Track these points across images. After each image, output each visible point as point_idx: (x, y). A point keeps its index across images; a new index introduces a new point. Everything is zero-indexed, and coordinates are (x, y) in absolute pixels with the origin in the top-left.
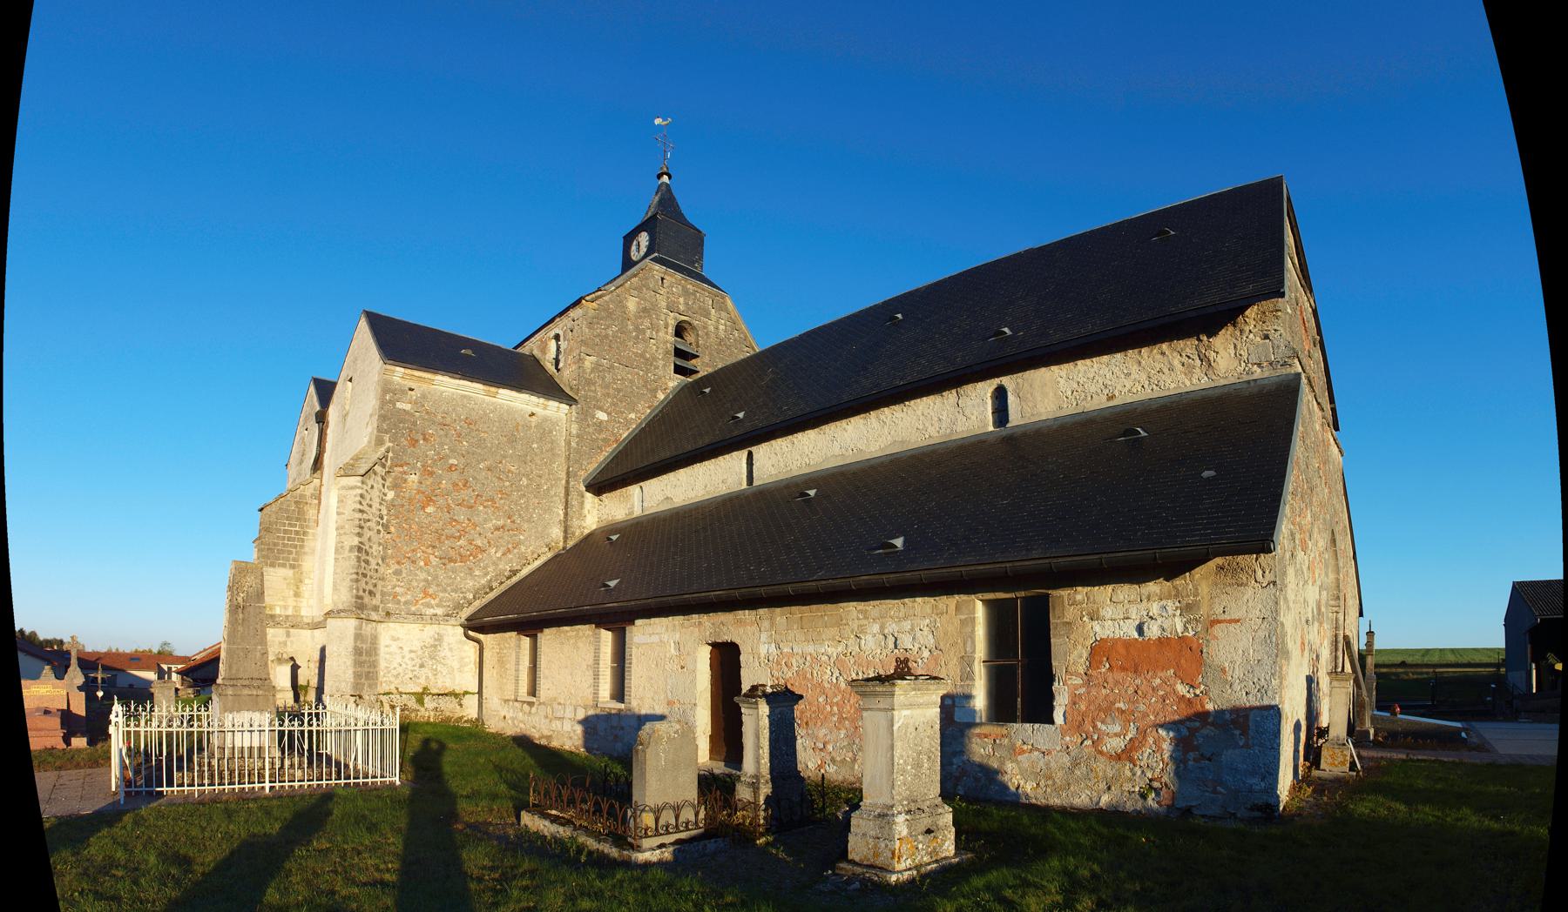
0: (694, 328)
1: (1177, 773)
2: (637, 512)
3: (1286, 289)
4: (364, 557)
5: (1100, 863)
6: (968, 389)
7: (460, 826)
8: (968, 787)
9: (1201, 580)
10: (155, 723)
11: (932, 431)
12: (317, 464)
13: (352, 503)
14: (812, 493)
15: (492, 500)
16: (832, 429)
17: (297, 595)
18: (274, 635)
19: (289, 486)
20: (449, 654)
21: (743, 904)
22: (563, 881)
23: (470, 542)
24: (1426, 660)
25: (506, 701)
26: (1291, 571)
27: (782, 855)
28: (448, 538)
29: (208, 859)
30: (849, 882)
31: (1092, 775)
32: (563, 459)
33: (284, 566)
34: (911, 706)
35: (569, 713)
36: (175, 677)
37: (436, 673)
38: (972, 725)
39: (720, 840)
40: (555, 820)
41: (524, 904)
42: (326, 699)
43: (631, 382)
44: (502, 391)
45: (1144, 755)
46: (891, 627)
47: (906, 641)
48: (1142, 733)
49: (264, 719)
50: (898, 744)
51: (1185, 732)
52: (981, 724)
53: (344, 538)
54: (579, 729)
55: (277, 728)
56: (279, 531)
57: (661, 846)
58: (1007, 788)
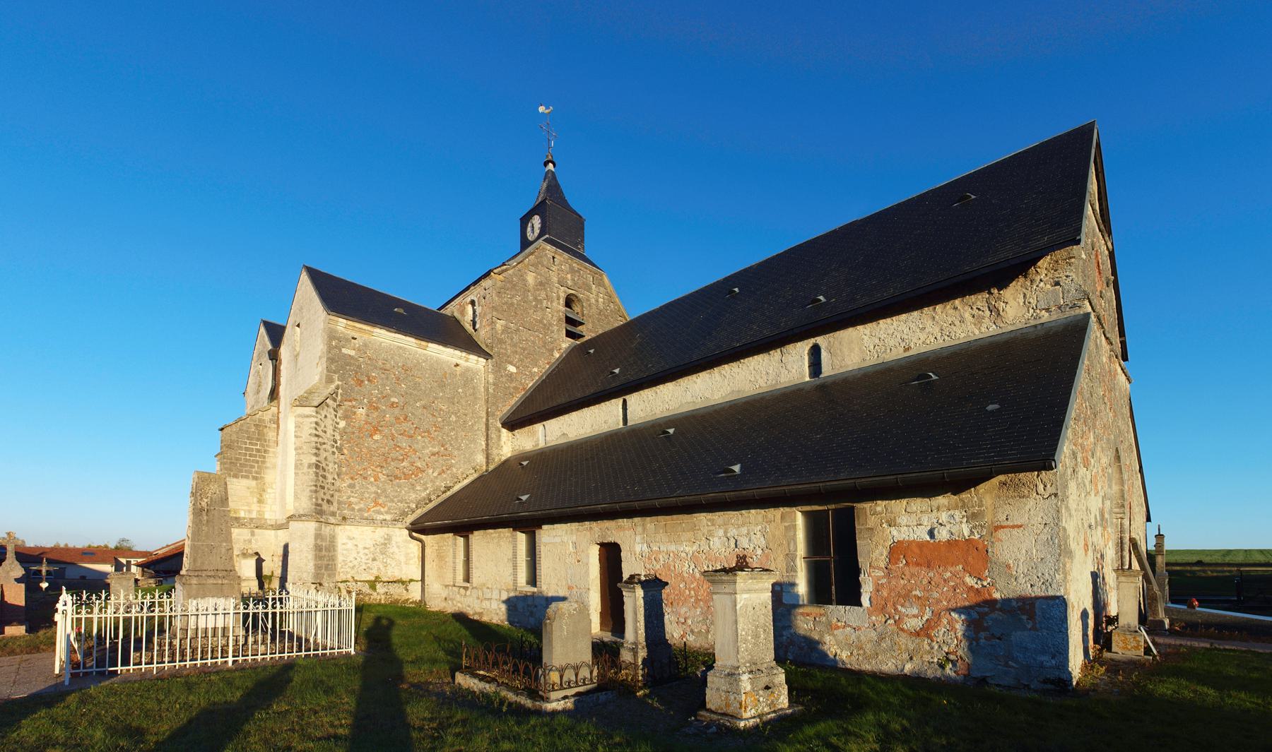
0: (579, 300)
1: (970, 648)
2: (542, 445)
3: (1083, 237)
4: (321, 473)
5: (909, 720)
6: (790, 348)
7: (405, 686)
8: (795, 653)
9: (986, 494)
10: (111, 610)
11: (762, 382)
12: (274, 394)
13: (308, 428)
15: (428, 432)
17: (260, 501)
19: (248, 411)
20: (396, 550)
21: (628, 744)
22: (489, 728)
23: (412, 464)
24: (1227, 559)
25: (447, 586)
26: (1072, 486)
27: (656, 704)
30: (708, 726)
31: (896, 647)
32: (483, 402)
33: (247, 477)
34: (749, 591)
35: (495, 595)
38: (797, 606)
40: (482, 678)
41: (457, 748)
42: (289, 586)
43: (533, 342)
44: (431, 345)
45: (940, 633)
46: (733, 532)
47: (744, 542)
48: (937, 616)
49: (229, 604)
50: (740, 620)
51: (975, 616)
52: (803, 606)
53: (302, 457)
54: (503, 607)
55: (242, 611)
56: (240, 448)
57: (565, 697)
58: (826, 655)
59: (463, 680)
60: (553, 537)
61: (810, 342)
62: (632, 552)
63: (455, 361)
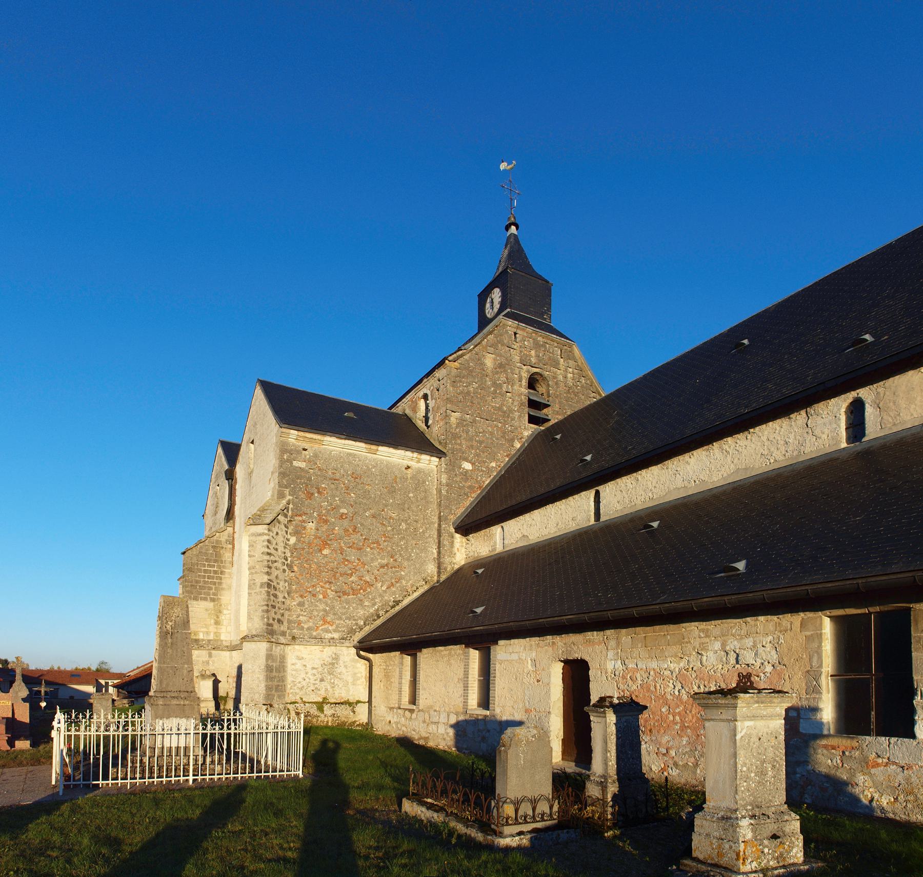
2: (499, 549)
4: (273, 592)
7: (351, 812)
12: (230, 515)
13: (261, 548)
14: (655, 524)
15: (378, 543)
16: (674, 464)
17: (217, 623)
18: (198, 655)
19: (207, 533)
22: (437, 859)
25: (391, 708)
27: (628, 848)
28: (341, 575)
29: (136, 840)
32: (435, 506)
33: (205, 599)
34: (754, 717)
35: (443, 719)
36: (111, 690)
37: (333, 686)
39: (572, 831)
40: (430, 807)
42: (243, 707)
43: (491, 433)
44: (380, 448)
46: (733, 644)
47: (748, 657)
49: (190, 724)
52: (828, 736)
53: (255, 576)
54: (451, 732)
55: (201, 731)
56: (200, 570)
57: (520, 833)
59: (409, 807)
60: (511, 654)
61: (851, 396)
62: (603, 670)
63: (406, 463)
